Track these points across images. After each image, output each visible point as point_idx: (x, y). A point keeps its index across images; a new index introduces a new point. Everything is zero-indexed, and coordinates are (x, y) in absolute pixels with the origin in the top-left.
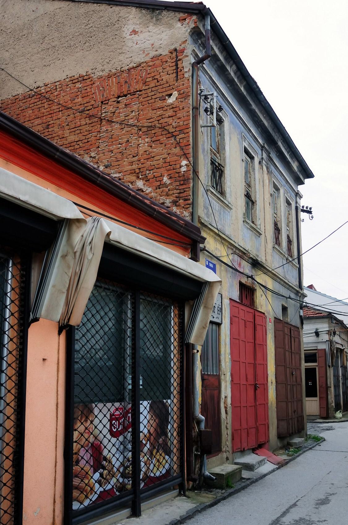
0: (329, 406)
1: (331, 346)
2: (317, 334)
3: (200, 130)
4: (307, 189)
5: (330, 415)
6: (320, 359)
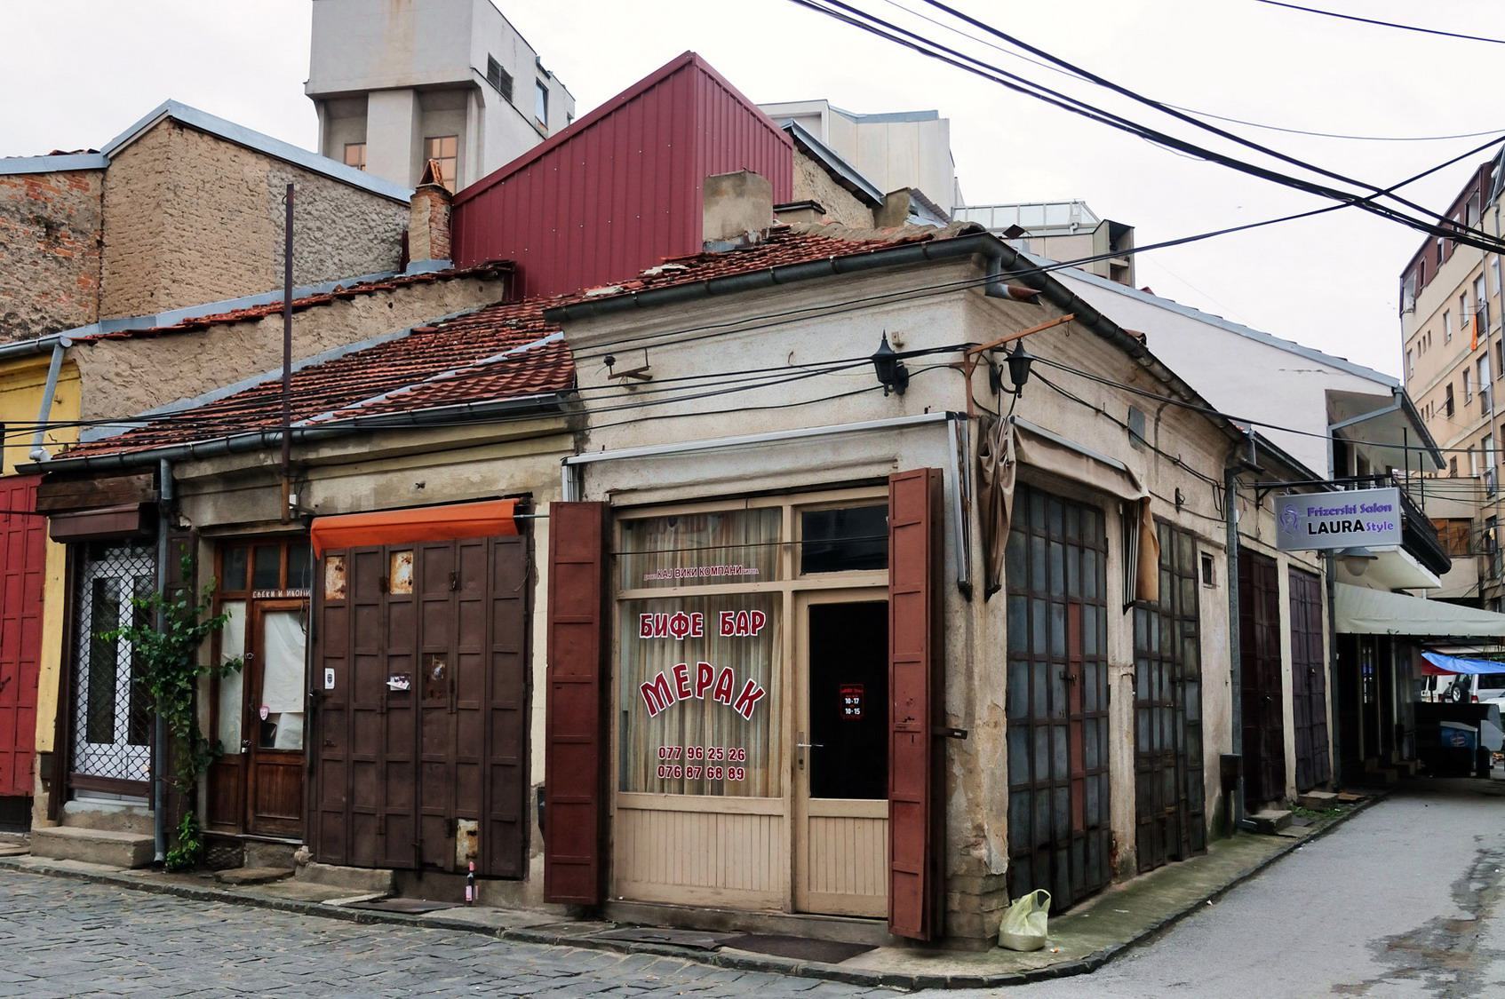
0: (957, 864)
1: (984, 450)
2: (892, 370)
3: (922, 656)
4: (941, 116)
5: (961, 923)
6: (908, 545)
